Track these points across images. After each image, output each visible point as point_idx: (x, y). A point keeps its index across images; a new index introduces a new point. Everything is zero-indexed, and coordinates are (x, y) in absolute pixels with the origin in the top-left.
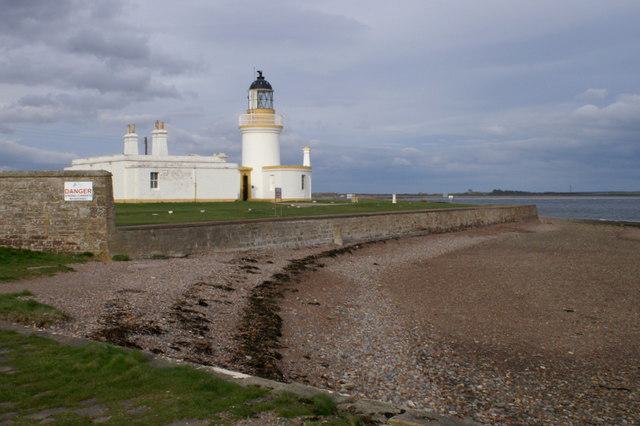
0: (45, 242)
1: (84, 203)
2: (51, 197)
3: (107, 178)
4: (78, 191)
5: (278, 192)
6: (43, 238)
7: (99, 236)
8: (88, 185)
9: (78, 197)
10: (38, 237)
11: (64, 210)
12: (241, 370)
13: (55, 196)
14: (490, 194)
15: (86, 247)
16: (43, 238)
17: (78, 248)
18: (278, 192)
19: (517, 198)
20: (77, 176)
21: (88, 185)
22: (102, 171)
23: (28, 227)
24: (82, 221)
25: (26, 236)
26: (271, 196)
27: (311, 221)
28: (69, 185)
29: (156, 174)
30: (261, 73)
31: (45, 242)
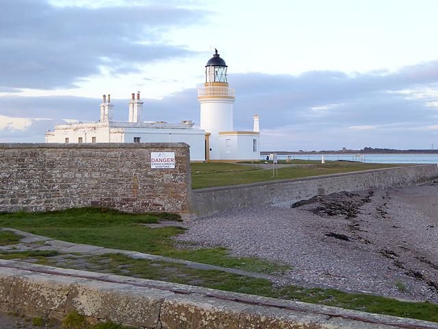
0: (134, 204)
1: (167, 171)
2: (139, 165)
3: (185, 149)
4: (163, 160)
5: (80, 139)
6: (133, 200)
7: (180, 198)
8: (171, 155)
9: (163, 165)
10: (128, 200)
11: (151, 176)
12: (363, 310)
13: (143, 164)
14: (362, 152)
15: (169, 208)
16: (133, 200)
17: (163, 209)
18: (80, 139)
19: (137, 132)
20: (161, 147)
21: (171, 155)
22: (183, 143)
23: (120, 190)
24: (166, 186)
25: (118, 199)
26: (76, 141)
27: (305, 182)
28: (155, 155)
29: (139, 138)
30: (216, 51)
31: (134, 204)
